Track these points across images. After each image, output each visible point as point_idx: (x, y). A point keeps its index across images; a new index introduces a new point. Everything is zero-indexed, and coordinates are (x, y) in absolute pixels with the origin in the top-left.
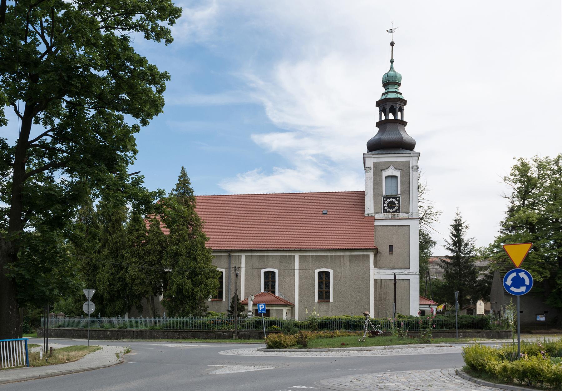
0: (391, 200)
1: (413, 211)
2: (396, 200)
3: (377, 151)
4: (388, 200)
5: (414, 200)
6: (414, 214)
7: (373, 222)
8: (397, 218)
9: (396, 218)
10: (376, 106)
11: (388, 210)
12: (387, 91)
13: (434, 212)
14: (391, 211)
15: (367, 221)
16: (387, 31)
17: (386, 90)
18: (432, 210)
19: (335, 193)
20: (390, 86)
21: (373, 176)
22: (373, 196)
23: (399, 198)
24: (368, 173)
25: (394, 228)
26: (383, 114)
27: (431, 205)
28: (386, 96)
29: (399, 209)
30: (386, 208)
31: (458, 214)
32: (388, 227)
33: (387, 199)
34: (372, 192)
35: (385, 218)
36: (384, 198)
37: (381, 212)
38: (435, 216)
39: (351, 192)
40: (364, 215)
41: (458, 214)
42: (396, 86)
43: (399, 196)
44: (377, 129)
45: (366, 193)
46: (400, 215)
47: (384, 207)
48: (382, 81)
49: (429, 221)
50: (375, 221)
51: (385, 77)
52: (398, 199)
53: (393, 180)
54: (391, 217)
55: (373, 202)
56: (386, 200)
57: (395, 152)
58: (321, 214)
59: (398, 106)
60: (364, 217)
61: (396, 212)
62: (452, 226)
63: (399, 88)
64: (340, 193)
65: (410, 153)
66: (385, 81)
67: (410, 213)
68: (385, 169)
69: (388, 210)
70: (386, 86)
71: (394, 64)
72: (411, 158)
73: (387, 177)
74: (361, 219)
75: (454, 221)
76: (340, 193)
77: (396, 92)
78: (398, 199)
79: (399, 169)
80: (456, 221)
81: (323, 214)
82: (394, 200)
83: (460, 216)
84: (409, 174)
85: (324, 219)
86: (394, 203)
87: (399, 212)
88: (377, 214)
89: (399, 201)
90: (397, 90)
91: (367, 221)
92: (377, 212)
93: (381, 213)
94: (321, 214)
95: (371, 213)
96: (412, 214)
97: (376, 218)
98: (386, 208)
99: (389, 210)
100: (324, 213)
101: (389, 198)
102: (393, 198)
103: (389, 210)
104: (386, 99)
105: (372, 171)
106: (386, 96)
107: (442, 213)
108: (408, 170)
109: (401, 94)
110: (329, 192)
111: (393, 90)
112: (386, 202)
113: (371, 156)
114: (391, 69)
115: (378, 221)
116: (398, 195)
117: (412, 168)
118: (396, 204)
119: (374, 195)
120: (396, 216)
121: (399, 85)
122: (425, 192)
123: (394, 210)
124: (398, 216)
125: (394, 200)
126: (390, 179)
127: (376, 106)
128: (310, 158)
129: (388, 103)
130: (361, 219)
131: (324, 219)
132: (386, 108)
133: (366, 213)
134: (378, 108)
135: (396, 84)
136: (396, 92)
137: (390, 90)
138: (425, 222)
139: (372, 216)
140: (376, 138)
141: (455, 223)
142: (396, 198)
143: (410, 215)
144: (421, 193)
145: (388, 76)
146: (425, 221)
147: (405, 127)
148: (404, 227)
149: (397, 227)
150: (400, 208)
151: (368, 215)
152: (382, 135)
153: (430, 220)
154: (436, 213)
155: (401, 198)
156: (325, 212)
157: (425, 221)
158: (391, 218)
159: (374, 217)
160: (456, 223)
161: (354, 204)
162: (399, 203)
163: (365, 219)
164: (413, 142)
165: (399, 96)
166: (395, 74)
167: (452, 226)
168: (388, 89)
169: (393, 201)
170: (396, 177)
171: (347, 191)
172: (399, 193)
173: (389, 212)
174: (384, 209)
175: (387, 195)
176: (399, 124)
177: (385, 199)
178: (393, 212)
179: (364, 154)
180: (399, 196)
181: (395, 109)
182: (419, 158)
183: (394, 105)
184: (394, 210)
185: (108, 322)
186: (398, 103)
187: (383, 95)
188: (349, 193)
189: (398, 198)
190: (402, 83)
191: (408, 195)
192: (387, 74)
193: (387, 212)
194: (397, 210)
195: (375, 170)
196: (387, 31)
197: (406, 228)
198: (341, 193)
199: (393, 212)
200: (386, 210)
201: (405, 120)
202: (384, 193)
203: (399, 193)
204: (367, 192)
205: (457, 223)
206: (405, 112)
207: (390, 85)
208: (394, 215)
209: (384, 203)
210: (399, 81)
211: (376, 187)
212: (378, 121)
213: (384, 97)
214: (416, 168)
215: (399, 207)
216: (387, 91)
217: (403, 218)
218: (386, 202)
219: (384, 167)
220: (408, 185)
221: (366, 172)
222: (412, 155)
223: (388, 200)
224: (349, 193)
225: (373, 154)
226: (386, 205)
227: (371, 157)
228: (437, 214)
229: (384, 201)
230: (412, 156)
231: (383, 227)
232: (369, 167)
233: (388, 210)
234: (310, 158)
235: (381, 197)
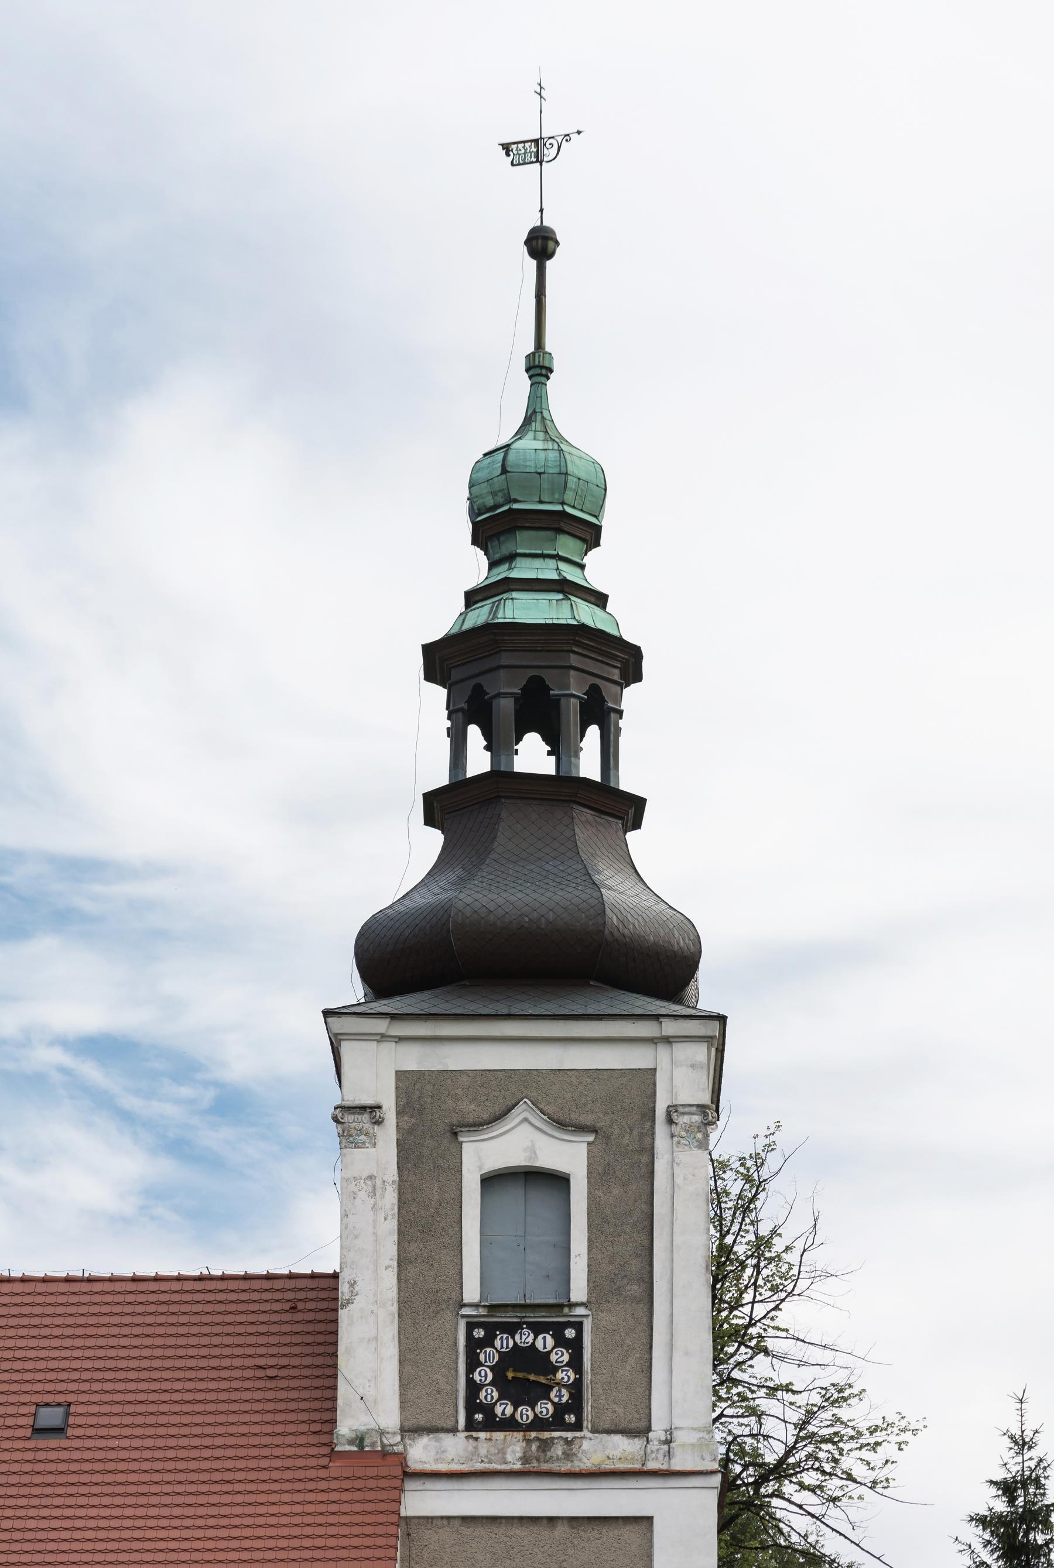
0: (525, 1338)
1: (677, 1422)
2: (561, 1341)
3: (426, 995)
4: (503, 1342)
5: (679, 1342)
6: (680, 1437)
7: (393, 1495)
8: (566, 1467)
9: (555, 1467)
10: (430, 676)
11: (504, 1409)
12: (502, 572)
13: (863, 1426)
14: (525, 1414)
15: (346, 1484)
16: (507, 148)
17: (492, 565)
18: (844, 1413)
19: (131, 1286)
20: (523, 541)
21: (391, 1173)
22: (395, 1308)
23: (579, 1327)
24: (357, 1145)
25: (544, 1533)
26: (474, 732)
27: (840, 1378)
28: (494, 612)
29: (576, 1404)
30: (489, 1394)
31: (1022, 1444)
32: (500, 1530)
33: (492, 1330)
34: (389, 1280)
35: (479, 1466)
36: (471, 1327)
37: (449, 1424)
38: (865, 1454)
39: (112, 1279)
40: (330, 1444)
41: (1022, 1444)
42: (567, 545)
43: (580, 1311)
44: (435, 839)
45: (344, 1289)
46: (586, 1445)
47: (473, 1388)
48: (465, 506)
49: (833, 1486)
50: (410, 1485)
51: (483, 475)
52: (570, 1333)
53: (541, 1200)
54: (525, 1459)
55: (391, 1351)
56: (488, 1341)
57: (553, 1008)
58: (20, 1433)
59: (576, 688)
60: (333, 1454)
61: (557, 1422)
62: (983, 1521)
63: (591, 558)
64: (165, 1286)
65: (657, 1017)
66: (490, 502)
67: (658, 1432)
68: (478, 1125)
69: (504, 1409)
70: (497, 535)
71: (553, 385)
72: (663, 1051)
73: (491, 1181)
74: (312, 1474)
75: (993, 1491)
76: (165, 1286)
77: (564, 587)
78: (570, 1333)
79: (581, 1129)
80: (1008, 1488)
81: (38, 1431)
82: (545, 1342)
83: (1035, 1453)
84: (645, 1159)
85: (39, 1467)
86: (541, 1362)
87: (578, 1426)
88: (425, 1440)
89: (575, 1347)
90: (571, 574)
91: (346, 1484)
92: (422, 1421)
93: (454, 1430)
94: (20, 1433)
95: (382, 1433)
96: (668, 1442)
97: (414, 1465)
98: (489, 1394)
99: (509, 1410)
100: (42, 1423)
101: (511, 1329)
102: (538, 1329)
103: (509, 1410)
104: (488, 628)
105: (388, 1135)
106: (494, 612)
107: (915, 1432)
108: (641, 1135)
109: (600, 599)
110: (91, 1280)
111: (547, 571)
112: (489, 1356)
113: (381, 1026)
114: (528, 421)
115: (429, 1484)
116: (572, 1305)
117: (670, 1121)
118: (555, 1369)
119: (404, 1303)
120: (558, 1450)
121: (591, 536)
122: (802, 1284)
123: (545, 1408)
124: (568, 1456)
125: (545, 1342)
126: (513, 1197)
127: (430, 676)
128: (57, 1056)
129: (506, 659)
130: (312, 1474)
131: (39, 1467)
132: (492, 692)
133: (347, 1426)
134: (440, 694)
135: (560, 531)
136: (564, 587)
137: (523, 570)
138: (805, 1498)
139: (385, 1454)
140: (419, 900)
141: (1001, 1506)
142: (557, 1331)
143: (654, 1446)
144: (783, 1295)
145: (504, 471)
146: (802, 1486)
147: (631, 837)
148: (611, 1533)
149: (561, 1530)
150: (587, 1394)
151: (359, 1440)
152: (460, 883)
153: (836, 1482)
154: (873, 1430)
155: (595, 1328)
156: (51, 1417)
157: (802, 1486)
158: (518, 1466)
159: (402, 1457)
160: (1012, 1501)
161: (261, 1362)
162: (576, 1363)
163: (336, 1468)
164: (680, 942)
165: (586, 614)
166: (553, 455)
167: (983, 1521)
168: (511, 558)
169: (539, 1344)
170: (559, 1181)
171: (17, 1274)
172: (579, 1291)
173: (509, 1425)
174: (473, 1405)
175: (493, 1308)
176: (587, 814)
177: (479, 1333)
178: (539, 1424)
179: (327, 1013)
180: (580, 1311)
181: (555, 704)
182: (721, 1052)
183: (549, 676)
184: (545, 1408)
185: (839, 1523)
186: (574, 660)
187: (472, 598)
188: (232, 1285)
189: (569, 1325)
190: (609, 523)
191: (641, 1309)
192: (500, 456)
193: (493, 1424)
194: (560, 1410)
195: (411, 1131)
196: (507, 148)
197: (630, 1535)
198: (176, 1286)
199: (539, 1424)
200: (488, 1410)
201: (628, 782)
202: (472, 1292)
203: (579, 1291)
204: (352, 1284)
205: (1020, 1502)
206: (628, 726)
207: (521, 536)
208: (545, 1445)
209: (473, 1363)
210: (588, 506)
211: (413, 1248)
212: (442, 779)
213: (480, 616)
214: (697, 1119)
215: (576, 1389)
216: (502, 572)
217: (608, 1466)
218: (489, 1356)
219: (472, 1110)
220: (643, 1238)
221: (348, 1138)
222: (670, 1028)
223: (503, 1342)
224: (232, 1285)
225: (393, 1017)
226: (484, 1375)
227: (383, 1038)
228: (879, 1436)
229: (473, 1347)
230: (668, 1040)
231: (467, 1531)
232: (363, 1109)
233: (499, 1410)
234: (57, 1056)
235: (449, 1315)
